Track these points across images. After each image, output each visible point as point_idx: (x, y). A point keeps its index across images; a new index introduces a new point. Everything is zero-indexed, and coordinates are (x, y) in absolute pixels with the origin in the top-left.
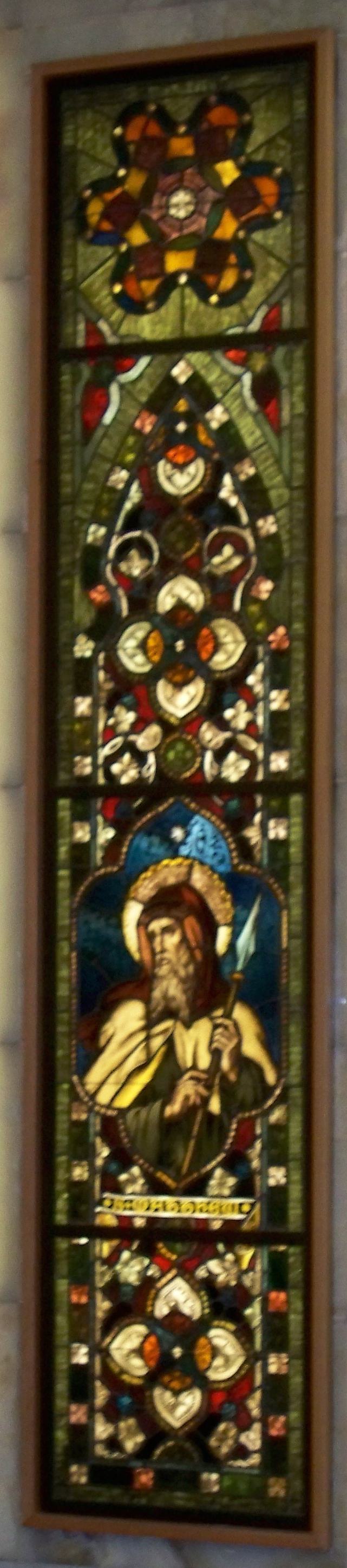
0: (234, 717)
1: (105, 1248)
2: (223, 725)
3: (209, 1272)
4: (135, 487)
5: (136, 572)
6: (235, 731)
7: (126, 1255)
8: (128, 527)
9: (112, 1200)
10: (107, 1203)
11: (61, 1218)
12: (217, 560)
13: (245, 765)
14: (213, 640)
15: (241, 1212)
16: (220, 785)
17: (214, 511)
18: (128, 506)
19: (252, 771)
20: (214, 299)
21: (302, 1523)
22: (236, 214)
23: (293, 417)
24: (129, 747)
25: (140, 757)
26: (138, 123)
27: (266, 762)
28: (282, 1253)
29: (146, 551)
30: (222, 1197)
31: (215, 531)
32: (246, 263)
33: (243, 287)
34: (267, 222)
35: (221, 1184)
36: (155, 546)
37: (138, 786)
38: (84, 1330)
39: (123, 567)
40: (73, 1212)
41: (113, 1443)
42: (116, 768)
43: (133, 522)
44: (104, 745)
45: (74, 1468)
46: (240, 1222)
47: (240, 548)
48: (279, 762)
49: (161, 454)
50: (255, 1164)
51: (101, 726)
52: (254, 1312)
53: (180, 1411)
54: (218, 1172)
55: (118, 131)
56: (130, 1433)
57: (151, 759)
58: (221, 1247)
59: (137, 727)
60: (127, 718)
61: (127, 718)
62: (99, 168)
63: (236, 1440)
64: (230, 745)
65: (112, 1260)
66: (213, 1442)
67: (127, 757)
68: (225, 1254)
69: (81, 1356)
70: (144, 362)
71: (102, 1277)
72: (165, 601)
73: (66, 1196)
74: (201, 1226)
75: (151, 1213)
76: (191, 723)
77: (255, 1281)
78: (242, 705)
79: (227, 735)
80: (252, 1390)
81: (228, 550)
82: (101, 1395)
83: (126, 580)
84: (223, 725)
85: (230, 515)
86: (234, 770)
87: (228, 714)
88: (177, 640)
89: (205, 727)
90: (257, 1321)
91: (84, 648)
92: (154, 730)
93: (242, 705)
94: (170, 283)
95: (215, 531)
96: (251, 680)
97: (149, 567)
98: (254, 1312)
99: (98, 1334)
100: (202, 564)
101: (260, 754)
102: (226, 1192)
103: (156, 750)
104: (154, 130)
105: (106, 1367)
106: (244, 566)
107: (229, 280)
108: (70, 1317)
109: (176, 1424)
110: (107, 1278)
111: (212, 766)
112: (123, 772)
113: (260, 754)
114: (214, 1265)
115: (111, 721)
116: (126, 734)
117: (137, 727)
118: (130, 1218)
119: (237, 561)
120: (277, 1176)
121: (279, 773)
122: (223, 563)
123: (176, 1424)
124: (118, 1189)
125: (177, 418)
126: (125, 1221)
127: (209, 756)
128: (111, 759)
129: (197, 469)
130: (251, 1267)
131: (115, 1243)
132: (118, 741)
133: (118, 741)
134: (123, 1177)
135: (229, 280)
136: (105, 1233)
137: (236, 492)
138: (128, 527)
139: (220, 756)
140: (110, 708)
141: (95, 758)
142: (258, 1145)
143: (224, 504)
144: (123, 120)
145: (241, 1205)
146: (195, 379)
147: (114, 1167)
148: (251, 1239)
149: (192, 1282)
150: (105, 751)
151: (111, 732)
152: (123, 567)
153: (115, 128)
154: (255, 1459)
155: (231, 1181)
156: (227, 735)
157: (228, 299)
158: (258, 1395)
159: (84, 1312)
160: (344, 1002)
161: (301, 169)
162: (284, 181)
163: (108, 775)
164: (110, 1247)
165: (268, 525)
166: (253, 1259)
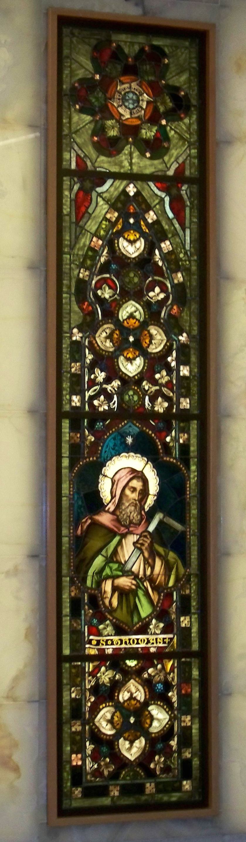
1: (90, 667)
2: (155, 382)
5: (107, 296)
7: (103, 669)
8: (101, 272)
9: (112, 640)
10: (94, 642)
11: (67, 651)
12: (151, 294)
14: (149, 338)
15: (164, 643)
16: (155, 415)
17: (149, 268)
18: (103, 260)
19: (170, 408)
21: (62, 812)
24: (103, 391)
25: (109, 397)
27: (178, 403)
31: (150, 279)
35: (156, 627)
37: (108, 414)
39: (99, 292)
40: (73, 648)
41: (97, 773)
42: (96, 403)
43: (105, 268)
44: (88, 390)
45: (185, 783)
46: (165, 648)
47: (164, 289)
48: (185, 403)
49: (120, 234)
50: (173, 616)
53: (134, 750)
56: (107, 765)
59: (108, 380)
60: (101, 376)
61: (101, 376)
62: (83, 70)
64: (158, 393)
65: (93, 674)
66: (152, 766)
67: (102, 398)
70: (109, 182)
74: (146, 652)
76: (138, 381)
77: (174, 678)
79: (157, 388)
81: (157, 290)
82: (89, 747)
83: (101, 301)
84: (155, 382)
85: (159, 271)
86: (161, 406)
87: (157, 376)
90: (175, 699)
91: (77, 336)
92: (116, 383)
95: (150, 279)
97: (114, 295)
98: (173, 696)
100: (143, 296)
102: (158, 632)
103: (117, 393)
105: (92, 731)
106: (166, 299)
109: (132, 758)
110: (93, 683)
112: (100, 406)
115: (93, 376)
116: (101, 384)
119: (162, 296)
120: (185, 622)
121: (185, 410)
123: (132, 758)
125: (129, 215)
128: (92, 398)
129: (141, 244)
130: (172, 670)
131: (96, 663)
132: (97, 387)
133: (97, 387)
134: (101, 627)
136: (91, 658)
137: (162, 259)
139: (153, 400)
140: (91, 371)
141: (83, 397)
145: (164, 639)
146: (138, 194)
148: (170, 656)
149: (124, 682)
150: (91, 393)
151: (92, 383)
155: (162, 625)
156: (157, 388)
163: (91, 405)
164: (94, 666)
165: (179, 277)
166: (173, 666)
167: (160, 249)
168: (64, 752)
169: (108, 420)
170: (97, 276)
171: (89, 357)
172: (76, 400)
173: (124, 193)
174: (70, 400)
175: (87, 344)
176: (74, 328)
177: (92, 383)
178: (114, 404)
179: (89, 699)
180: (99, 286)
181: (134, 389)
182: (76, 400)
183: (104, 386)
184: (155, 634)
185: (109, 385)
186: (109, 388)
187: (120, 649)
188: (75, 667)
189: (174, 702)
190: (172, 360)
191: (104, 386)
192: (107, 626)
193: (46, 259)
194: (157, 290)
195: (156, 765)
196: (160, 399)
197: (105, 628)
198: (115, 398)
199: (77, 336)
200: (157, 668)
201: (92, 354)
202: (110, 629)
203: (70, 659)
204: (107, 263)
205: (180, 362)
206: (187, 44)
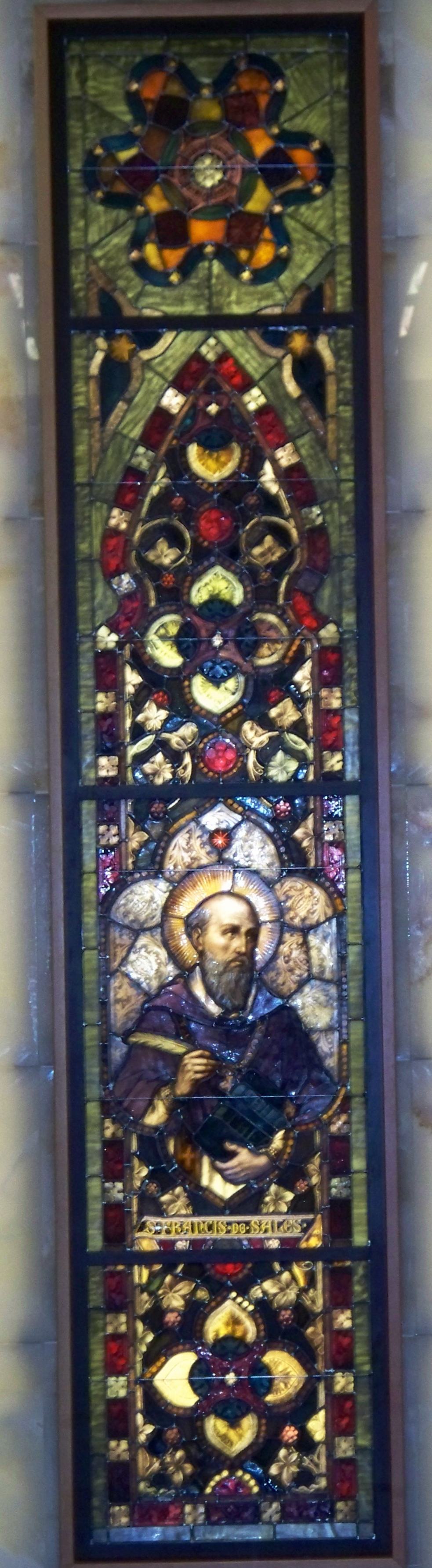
0: (280, 715)
1: (141, 1275)
3: (265, 1293)
4: (162, 471)
5: (166, 561)
6: (281, 729)
12: (257, 551)
13: (293, 765)
18: (155, 490)
20: (246, 275)
22: (271, 184)
23: (313, 651)
24: (161, 745)
25: (175, 758)
26: (158, 79)
28: (349, 1267)
29: (176, 540)
30: (280, 1213)
32: (282, 237)
33: (280, 264)
34: (305, 196)
36: (187, 535)
37: (174, 788)
38: (121, 1362)
39: (151, 556)
41: (160, 1479)
43: (161, 504)
47: (282, 535)
51: (128, 723)
52: (315, 1332)
54: (273, 1188)
55: (135, 86)
56: (179, 1466)
57: (187, 759)
58: (277, 1266)
59: (169, 725)
63: (299, 1464)
64: (277, 744)
68: (281, 1273)
69: (118, 1387)
70: (168, 337)
71: (144, 1302)
72: (199, 594)
73: (77, 286)
75: (196, 1236)
77: (317, 1299)
78: (288, 703)
80: (314, 1411)
81: (269, 540)
84: (266, 723)
85: (270, 504)
87: (273, 712)
88: (213, 635)
89: (247, 726)
91: (108, 638)
93: (288, 703)
94: (195, 256)
96: (298, 677)
99: (139, 1367)
101: (310, 753)
102: (284, 1208)
104: (175, 89)
106: (287, 559)
107: (265, 254)
108: (107, 1349)
111: (255, 766)
113: (310, 753)
114: (269, 1286)
116: (157, 732)
117: (169, 725)
118: (173, 1242)
122: (263, 554)
124: (160, 1211)
126: (168, 1245)
127: (252, 757)
132: (148, 740)
133: (148, 740)
134: (165, 1198)
135: (265, 254)
136: (146, 1259)
138: (151, 514)
139: (264, 757)
140: (138, 708)
142: (317, 1160)
143: (265, 494)
144: (139, 72)
147: (153, 1187)
151: (139, 731)
152: (151, 556)
153: (130, 253)
154: (323, 1483)
155: (289, 1196)
157: (261, 276)
158: (322, 1415)
159: (125, 1341)
160: (429, 919)
161: (343, 140)
162: (324, 155)
167: (275, 462)
168: (124, 1029)
169: (176, 799)
170: (145, 522)
171: (132, 679)
172: (106, 767)
173: (197, 357)
174: (96, 766)
175: (134, 1145)
176: (100, 626)
177: (139, 731)
178: (185, 768)
179: (143, 1338)
180: (148, 542)
181: (210, 770)
182: (106, 767)
183: (165, 735)
184: (276, 1213)
185: (175, 733)
186: (174, 739)
187: (204, 1241)
188: (112, 1274)
189: (318, 1346)
190: (303, 676)
191: (165, 735)
192: (178, 1197)
193: (39, 503)
194: (269, 540)
195: (281, 1468)
196: (280, 755)
197: (173, 1201)
198: (187, 759)
199: (108, 638)
200: (279, 1281)
201: (136, 690)
202: (182, 1202)
203: (101, 1259)
204: (166, 494)
205: (320, 681)
206: (128, 932)
